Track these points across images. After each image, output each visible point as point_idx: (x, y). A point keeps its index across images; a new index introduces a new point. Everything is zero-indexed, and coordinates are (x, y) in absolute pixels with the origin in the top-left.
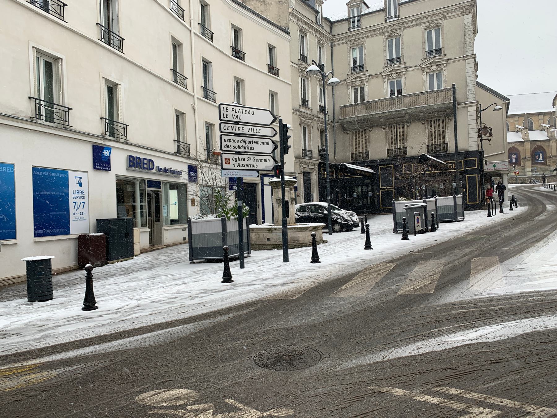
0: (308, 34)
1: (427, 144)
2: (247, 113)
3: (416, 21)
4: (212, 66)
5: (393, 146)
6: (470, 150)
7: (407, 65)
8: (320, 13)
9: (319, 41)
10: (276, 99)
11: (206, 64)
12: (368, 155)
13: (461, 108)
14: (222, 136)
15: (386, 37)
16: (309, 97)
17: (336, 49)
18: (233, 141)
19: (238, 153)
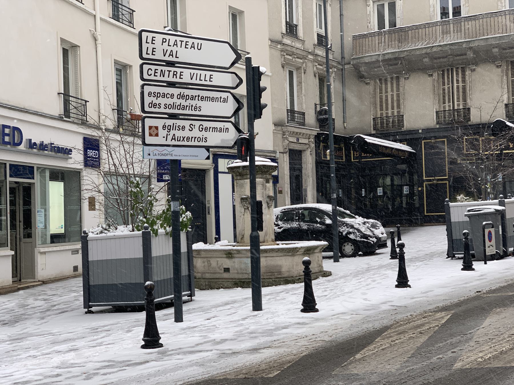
1: (506, 102)
5: (447, 104)
14: (145, 87)
16: (298, 19)
18: (164, 96)
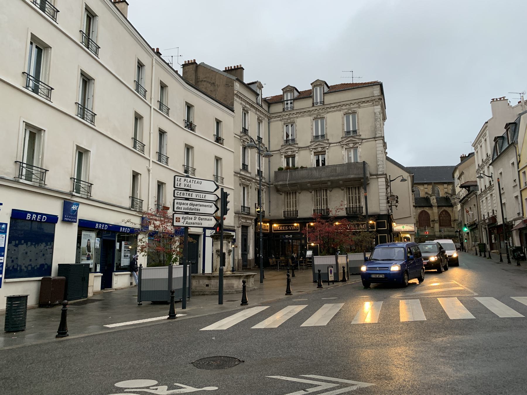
0: (249, 112)
2: (196, 183)
3: (337, 107)
4: (167, 136)
5: (318, 207)
6: (381, 214)
7: (330, 141)
8: (260, 96)
9: (258, 117)
10: (220, 164)
11: (162, 133)
12: (298, 213)
13: (373, 178)
14: (175, 200)
15: (313, 118)
16: (248, 162)
17: (273, 125)
18: (184, 204)
19: (187, 213)
